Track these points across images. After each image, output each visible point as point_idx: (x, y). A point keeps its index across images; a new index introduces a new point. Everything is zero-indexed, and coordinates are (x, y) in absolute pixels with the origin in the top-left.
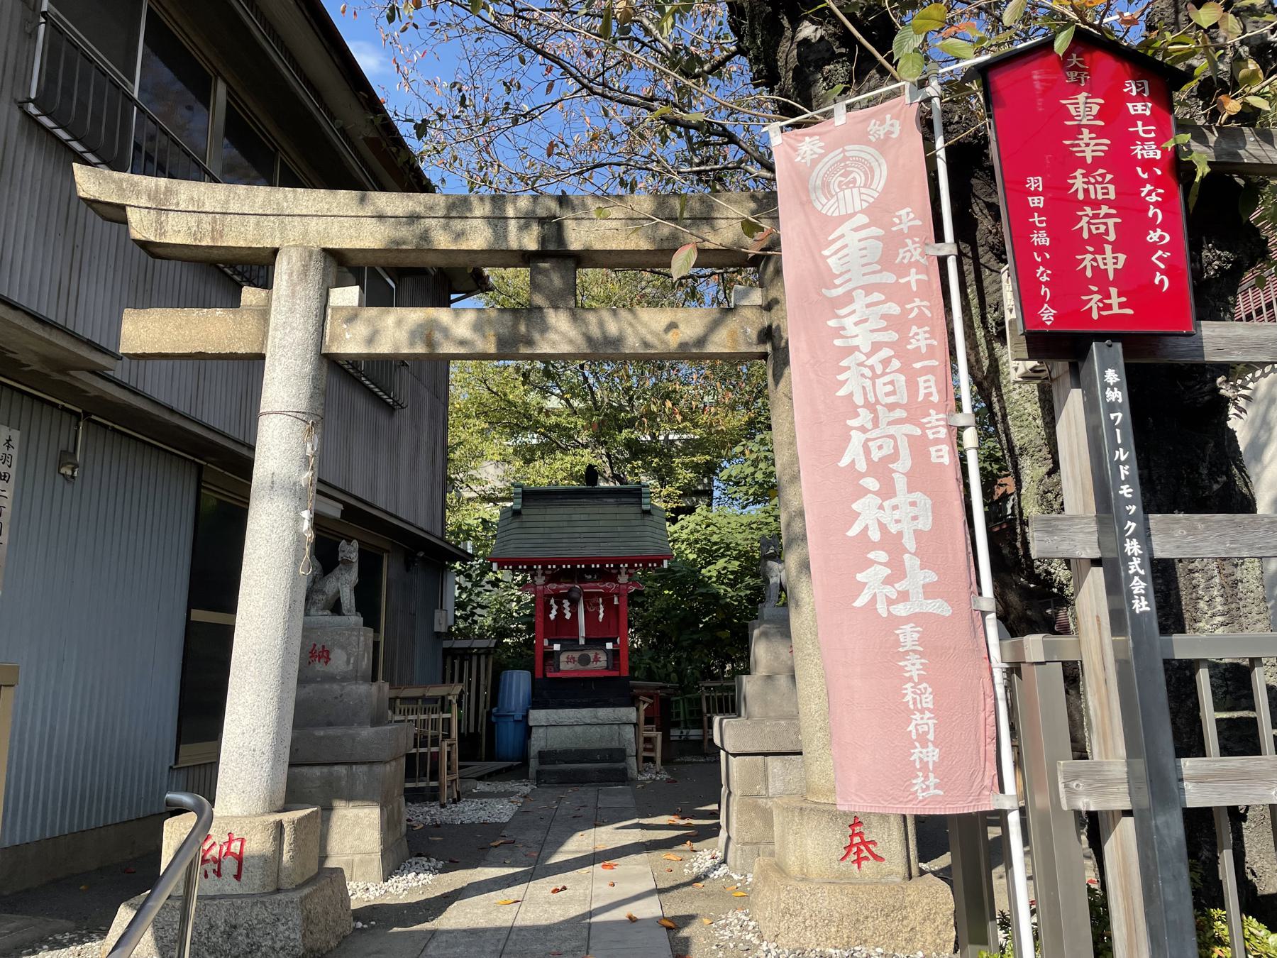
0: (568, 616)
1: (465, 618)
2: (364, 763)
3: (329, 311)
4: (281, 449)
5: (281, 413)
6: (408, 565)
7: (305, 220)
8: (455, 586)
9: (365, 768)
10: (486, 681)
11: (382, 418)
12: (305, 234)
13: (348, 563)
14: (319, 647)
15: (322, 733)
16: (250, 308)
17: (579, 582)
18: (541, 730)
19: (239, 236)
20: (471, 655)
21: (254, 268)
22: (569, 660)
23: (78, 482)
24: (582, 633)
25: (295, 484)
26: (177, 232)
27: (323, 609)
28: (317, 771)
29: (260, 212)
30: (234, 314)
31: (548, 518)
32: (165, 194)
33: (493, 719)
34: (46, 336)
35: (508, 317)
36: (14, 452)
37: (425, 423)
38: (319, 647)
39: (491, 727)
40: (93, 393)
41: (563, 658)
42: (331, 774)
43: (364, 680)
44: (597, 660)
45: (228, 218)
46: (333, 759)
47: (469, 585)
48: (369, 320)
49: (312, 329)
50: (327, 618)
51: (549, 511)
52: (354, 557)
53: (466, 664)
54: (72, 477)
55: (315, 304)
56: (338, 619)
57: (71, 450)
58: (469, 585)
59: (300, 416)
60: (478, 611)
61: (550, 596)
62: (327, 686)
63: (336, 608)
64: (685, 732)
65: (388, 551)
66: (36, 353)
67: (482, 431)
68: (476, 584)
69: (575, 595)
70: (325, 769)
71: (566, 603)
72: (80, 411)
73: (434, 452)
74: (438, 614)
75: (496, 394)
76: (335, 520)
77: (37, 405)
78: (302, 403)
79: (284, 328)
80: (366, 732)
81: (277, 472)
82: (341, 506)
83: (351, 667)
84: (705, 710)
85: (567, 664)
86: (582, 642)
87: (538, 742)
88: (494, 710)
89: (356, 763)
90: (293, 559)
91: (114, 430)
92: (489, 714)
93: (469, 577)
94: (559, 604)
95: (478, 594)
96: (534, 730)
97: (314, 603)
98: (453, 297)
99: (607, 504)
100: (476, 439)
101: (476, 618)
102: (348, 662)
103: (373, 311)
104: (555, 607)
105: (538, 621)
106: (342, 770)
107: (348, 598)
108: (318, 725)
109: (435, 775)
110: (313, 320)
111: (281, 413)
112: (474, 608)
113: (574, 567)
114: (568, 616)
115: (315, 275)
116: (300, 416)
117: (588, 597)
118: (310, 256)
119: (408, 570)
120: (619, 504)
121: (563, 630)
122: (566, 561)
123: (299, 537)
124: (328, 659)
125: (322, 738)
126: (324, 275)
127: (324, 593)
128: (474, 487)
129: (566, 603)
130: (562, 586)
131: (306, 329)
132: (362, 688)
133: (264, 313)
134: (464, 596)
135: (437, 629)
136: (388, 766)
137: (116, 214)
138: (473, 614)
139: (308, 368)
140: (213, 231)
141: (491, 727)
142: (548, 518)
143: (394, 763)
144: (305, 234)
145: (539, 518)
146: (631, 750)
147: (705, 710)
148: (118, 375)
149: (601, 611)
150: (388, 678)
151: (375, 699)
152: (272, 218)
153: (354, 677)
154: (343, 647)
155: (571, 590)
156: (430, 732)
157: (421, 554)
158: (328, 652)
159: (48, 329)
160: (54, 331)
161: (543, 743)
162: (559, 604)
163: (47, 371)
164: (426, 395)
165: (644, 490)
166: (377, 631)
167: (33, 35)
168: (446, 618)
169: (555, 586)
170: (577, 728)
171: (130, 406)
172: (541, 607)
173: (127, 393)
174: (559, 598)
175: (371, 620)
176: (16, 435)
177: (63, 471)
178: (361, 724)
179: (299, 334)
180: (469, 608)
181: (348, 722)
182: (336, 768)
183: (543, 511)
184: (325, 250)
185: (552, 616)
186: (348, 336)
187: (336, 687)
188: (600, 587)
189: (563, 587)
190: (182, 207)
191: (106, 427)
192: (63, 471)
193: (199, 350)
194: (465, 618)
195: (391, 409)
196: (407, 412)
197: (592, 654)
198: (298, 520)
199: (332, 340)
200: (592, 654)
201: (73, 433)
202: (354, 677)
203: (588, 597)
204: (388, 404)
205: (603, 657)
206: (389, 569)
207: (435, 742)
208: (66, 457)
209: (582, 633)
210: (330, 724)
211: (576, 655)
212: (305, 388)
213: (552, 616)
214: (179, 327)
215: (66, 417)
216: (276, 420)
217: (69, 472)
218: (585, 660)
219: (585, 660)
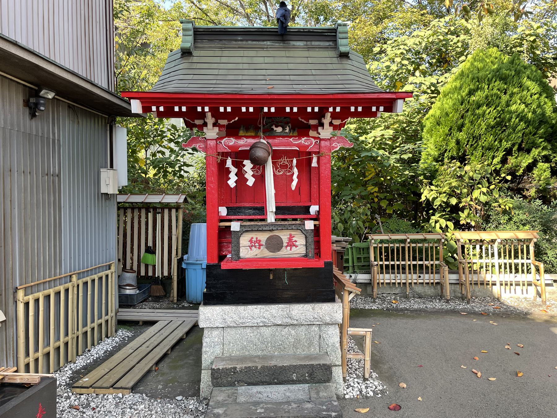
0: (251, 182)
6: (32, 107)
10: (177, 233)
17: (268, 137)
18: (215, 333)
22: (253, 244)
24: (271, 206)
31: (224, 60)
33: (184, 266)
39: (182, 272)
41: (244, 240)
44: (291, 244)
47: (177, 149)
51: (226, 53)
53: (159, 217)
60: (185, 168)
61: (225, 155)
64: (353, 276)
69: (260, 153)
71: (248, 165)
74: (106, 175)
84: (372, 258)
85: (250, 249)
86: (271, 218)
87: (212, 350)
88: (185, 257)
92: (180, 261)
94: (239, 165)
96: (206, 332)
99: (295, 47)
101: (182, 173)
104: (234, 170)
105: (212, 186)
113: (258, 110)
114: (251, 182)
117: (276, 155)
119: (33, 115)
120: (309, 48)
121: (246, 203)
122: (248, 100)
129: (248, 165)
130: (241, 142)
135: (103, 190)
138: (181, 169)
141: (182, 272)
142: (224, 60)
145: (217, 60)
146: (335, 358)
147: (372, 258)
149: (295, 177)
155: (253, 147)
161: (218, 351)
162: (239, 165)
165: (340, 29)
169: (232, 141)
170: (263, 330)
172: (214, 169)
174: (239, 157)
183: (219, 53)
185: (232, 183)
188: (295, 143)
189: (244, 143)
197: (284, 236)
200: (284, 236)
203: (276, 155)
205: (300, 240)
209: (271, 206)
211: (263, 237)
213: (232, 183)
218: (275, 244)
219: (275, 244)
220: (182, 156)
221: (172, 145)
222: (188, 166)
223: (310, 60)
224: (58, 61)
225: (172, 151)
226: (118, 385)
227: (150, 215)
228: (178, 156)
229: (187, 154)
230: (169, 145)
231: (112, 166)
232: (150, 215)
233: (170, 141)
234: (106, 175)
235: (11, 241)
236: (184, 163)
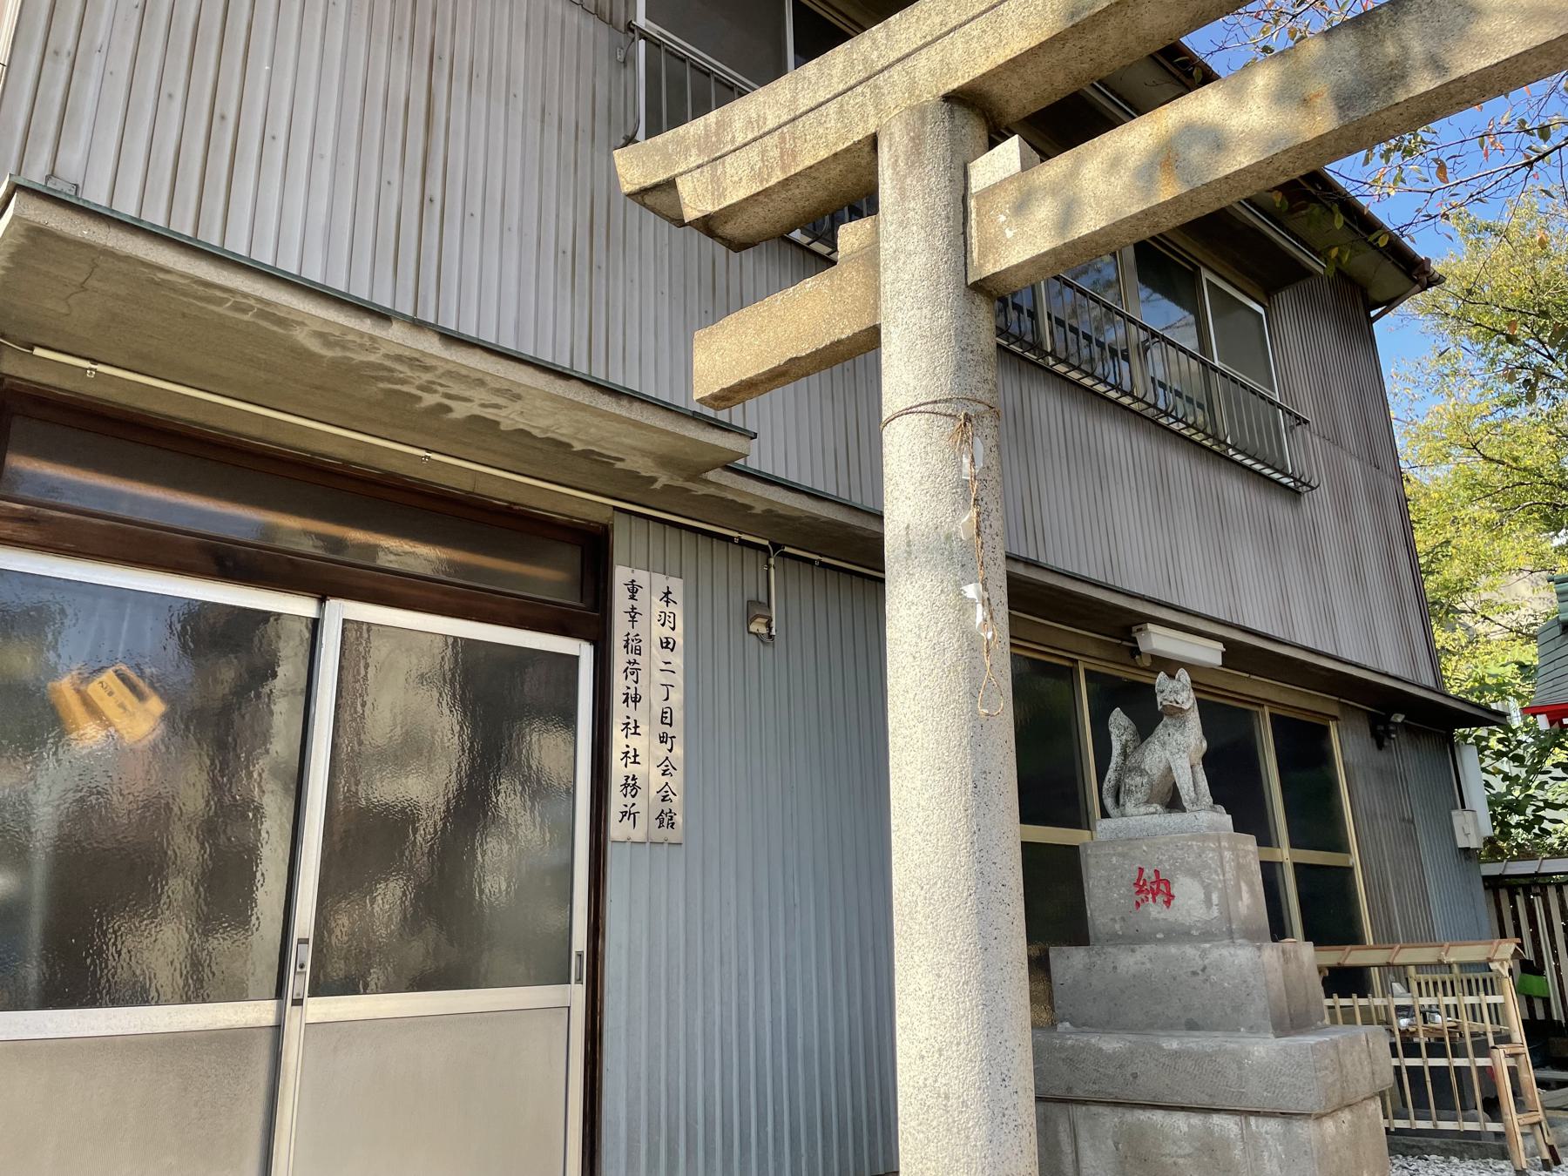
1: (1528, 827)
2: (1272, 1115)
3: (972, 203)
4: (919, 484)
5: (908, 411)
6: (1380, 738)
7: (909, 63)
8: (1481, 774)
9: (1272, 1126)
11: (1280, 510)
12: (912, 87)
13: (1176, 712)
14: (1149, 873)
15: (1173, 1044)
16: (852, 257)
19: (818, 145)
20: (1544, 887)
21: (848, 194)
23: (780, 641)
25: (948, 537)
26: (738, 182)
27: (1148, 802)
28: (1180, 1122)
29: (841, 87)
30: (831, 278)
32: (717, 134)
34: (624, 413)
35: (1347, 43)
36: (678, 610)
37: (1363, 513)
38: (1149, 873)
40: (759, 508)
42: (1209, 1131)
43: (1251, 936)
45: (799, 123)
46: (1205, 1101)
48: (1054, 190)
49: (941, 244)
50: (1156, 819)
52: (1187, 699)
54: (770, 637)
55: (942, 200)
56: (1176, 818)
57: (763, 598)
58: (1522, 773)
59: (941, 408)
60: (1548, 813)
62: (1173, 950)
63: (1173, 802)
65: (1335, 718)
66: (645, 453)
67: (1489, 526)
68: (1535, 770)
70: (1196, 1120)
72: (766, 543)
73: (1391, 557)
74: (1458, 818)
75: (1500, 462)
76: (1211, 670)
77: (703, 542)
78: (944, 385)
79: (896, 260)
80: (1264, 1048)
81: (913, 522)
82: (1220, 646)
83: (1215, 912)
89: (1257, 1114)
90: (966, 686)
91: (823, 565)
93: (1518, 759)
95: (1541, 786)
97: (1129, 792)
98: (1373, 313)
100: (1482, 540)
101: (1546, 825)
102: (1208, 901)
103: (1060, 164)
106: (1227, 1125)
107: (1191, 779)
108: (1170, 1026)
109: (1492, 1107)
110: (942, 227)
111: (908, 411)
112: (1539, 809)
115: (936, 149)
116: (941, 408)
118: (923, 119)
119: (1380, 746)
123: (972, 644)
124: (1169, 898)
125: (1176, 1055)
126: (953, 142)
127: (1142, 772)
128: (1496, 618)
131: (933, 247)
132: (1240, 956)
133: (871, 257)
134: (1516, 793)
135: (1462, 843)
136: (1329, 1125)
137: (658, 197)
139: (944, 316)
140: (782, 156)
143: (1346, 1116)
144: (912, 87)
148: (753, 464)
150: (1317, 934)
151: (1276, 978)
152: (859, 89)
153: (1226, 932)
154: (1194, 873)
156: (1467, 1025)
157: (1400, 718)
158: (1167, 883)
159: (625, 402)
160: (636, 405)
163: (679, 483)
164: (1354, 467)
166: (1265, 840)
167: (628, 61)
168: (1473, 827)
171: (816, 519)
173: (804, 498)
175: (1248, 815)
176: (676, 585)
177: (753, 628)
178: (1253, 1029)
179: (919, 261)
180: (1529, 810)
181: (1228, 1023)
182: (1216, 1119)
184: (949, 98)
186: (1009, 234)
187: (1190, 951)
190: (739, 141)
191: (811, 562)
192: (753, 628)
193: (789, 356)
194: (1528, 827)
195: (1293, 494)
196: (1323, 493)
198: (965, 606)
199: (983, 255)
201: (762, 578)
202: (1226, 932)
204: (1285, 486)
206: (1346, 747)
207: (1482, 1049)
208: (756, 608)
210: (1192, 1026)
212: (945, 356)
214: (758, 333)
215: (750, 554)
216: (901, 429)
217: (763, 630)
220: (1541, 786)
221: (1505, 765)
222: (1556, 807)
223: (1047, 447)
224: (1051, 563)
225: (1506, 777)
226: (649, 200)
227: (1520, 900)
228: (1529, 787)
229: (1551, 782)
230: (1498, 765)
231: (1463, 806)
232: (1520, 900)
233: (1499, 755)
234: (1458, 818)
235: (292, 54)
236: (1545, 801)
